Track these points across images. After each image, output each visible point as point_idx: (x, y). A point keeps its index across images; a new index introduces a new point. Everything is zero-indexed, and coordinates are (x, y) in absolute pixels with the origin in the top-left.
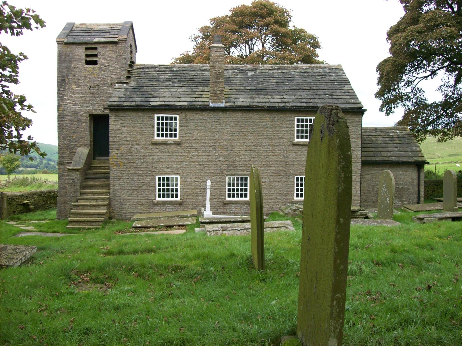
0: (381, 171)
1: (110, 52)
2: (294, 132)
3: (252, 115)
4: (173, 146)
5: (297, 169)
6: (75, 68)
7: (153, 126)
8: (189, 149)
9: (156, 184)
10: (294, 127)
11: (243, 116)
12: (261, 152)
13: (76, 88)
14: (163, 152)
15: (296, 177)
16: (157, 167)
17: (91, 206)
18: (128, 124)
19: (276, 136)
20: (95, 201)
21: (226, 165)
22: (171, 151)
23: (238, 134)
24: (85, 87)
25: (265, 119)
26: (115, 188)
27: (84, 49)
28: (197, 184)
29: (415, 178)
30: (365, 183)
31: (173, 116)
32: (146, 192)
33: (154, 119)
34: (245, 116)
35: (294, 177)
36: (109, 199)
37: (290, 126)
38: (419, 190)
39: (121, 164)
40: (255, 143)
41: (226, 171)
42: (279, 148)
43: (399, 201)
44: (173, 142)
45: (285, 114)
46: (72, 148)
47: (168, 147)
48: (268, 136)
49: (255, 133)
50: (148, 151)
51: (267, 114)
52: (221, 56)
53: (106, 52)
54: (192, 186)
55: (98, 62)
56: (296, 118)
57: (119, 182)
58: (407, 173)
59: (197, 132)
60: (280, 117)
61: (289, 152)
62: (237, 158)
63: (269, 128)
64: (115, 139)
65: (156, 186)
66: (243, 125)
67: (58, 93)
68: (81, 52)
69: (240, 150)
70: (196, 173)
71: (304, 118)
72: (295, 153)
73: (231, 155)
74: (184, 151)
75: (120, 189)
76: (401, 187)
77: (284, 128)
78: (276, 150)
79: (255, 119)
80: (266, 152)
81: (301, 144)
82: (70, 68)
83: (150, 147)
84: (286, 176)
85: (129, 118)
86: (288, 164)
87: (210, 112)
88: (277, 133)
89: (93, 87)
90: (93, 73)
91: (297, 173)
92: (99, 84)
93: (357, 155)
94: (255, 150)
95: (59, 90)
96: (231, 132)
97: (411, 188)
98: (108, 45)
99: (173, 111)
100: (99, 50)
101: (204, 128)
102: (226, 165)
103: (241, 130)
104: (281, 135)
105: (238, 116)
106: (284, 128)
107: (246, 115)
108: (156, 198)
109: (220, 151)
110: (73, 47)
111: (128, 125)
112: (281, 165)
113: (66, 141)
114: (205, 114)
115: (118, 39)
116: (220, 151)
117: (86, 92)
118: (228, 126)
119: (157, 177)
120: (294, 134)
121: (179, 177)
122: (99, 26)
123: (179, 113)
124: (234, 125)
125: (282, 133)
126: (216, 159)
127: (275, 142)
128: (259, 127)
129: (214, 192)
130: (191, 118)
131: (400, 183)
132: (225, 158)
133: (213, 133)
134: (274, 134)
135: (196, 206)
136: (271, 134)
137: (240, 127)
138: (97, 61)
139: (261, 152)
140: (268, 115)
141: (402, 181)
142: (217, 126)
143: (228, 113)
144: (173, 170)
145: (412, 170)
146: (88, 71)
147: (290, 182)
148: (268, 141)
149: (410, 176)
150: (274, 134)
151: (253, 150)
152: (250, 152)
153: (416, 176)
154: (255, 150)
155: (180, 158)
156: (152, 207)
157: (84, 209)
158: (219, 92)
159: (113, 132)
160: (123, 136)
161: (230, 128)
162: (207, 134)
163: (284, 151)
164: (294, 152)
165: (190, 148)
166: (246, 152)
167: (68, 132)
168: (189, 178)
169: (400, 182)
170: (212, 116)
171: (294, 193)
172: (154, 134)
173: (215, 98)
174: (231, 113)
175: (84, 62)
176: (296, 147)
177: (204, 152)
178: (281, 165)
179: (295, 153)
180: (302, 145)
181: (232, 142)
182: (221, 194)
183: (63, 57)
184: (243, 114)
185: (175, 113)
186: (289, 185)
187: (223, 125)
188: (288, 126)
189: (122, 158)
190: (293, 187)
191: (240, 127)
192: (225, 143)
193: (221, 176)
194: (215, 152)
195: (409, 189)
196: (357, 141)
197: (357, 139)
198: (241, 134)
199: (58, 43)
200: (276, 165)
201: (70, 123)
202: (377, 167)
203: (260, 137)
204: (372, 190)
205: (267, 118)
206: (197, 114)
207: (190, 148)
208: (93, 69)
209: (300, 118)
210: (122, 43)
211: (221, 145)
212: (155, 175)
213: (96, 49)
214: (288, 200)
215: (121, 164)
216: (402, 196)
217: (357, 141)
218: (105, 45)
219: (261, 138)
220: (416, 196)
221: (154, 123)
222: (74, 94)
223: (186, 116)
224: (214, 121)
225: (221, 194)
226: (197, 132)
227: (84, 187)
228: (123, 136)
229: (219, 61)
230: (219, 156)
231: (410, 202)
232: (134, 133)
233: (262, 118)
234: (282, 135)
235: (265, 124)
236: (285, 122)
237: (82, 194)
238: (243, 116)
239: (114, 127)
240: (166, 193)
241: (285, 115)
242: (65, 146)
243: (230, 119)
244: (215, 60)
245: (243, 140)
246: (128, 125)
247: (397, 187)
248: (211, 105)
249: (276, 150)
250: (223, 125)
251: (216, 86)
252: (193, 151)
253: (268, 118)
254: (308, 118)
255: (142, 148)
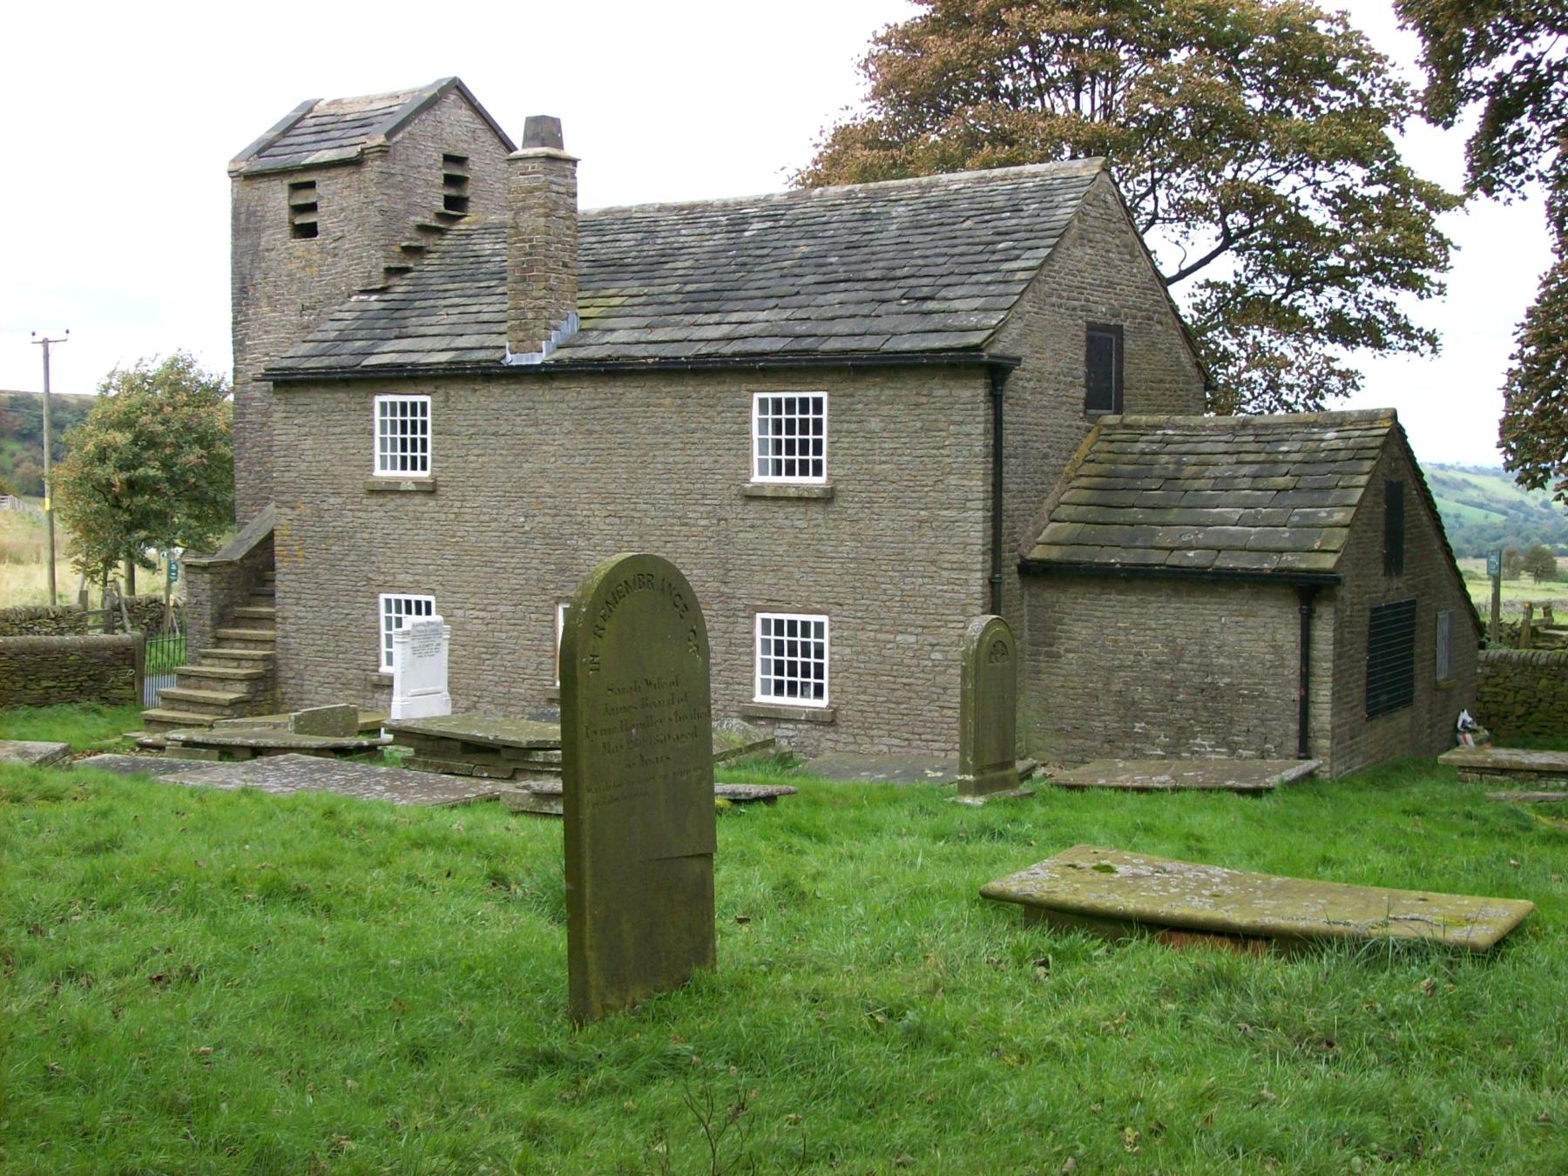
0: (1135, 610)
1: (346, 192)
2: (750, 449)
3: (621, 391)
4: (418, 500)
5: (759, 586)
6: (267, 250)
7: (372, 433)
8: (457, 510)
9: (378, 621)
10: (749, 432)
11: (597, 393)
12: (649, 521)
13: (272, 311)
14: (395, 518)
15: (759, 616)
16: (382, 565)
17: (214, 679)
18: (313, 427)
19: (693, 466)
20: (235, 664)
21: (553, 567)
22: (411, 515)
23: (582, 459)
24: (291, 307)
25: (660, 405)
26: (289, 627)
27: (286, 187)
28: (477, 626)
29: (1287, 646)
30: (1071, 655)
31: (811, 395)
32: (356, 645)
33: (371, 409)
34: (602, 396)
35: (752, 618)
36: (265, 659)
37: (735, 428)
38: (1305, 703)
39: (299, 553)
40: (632, 491)
41: (552, 586)
42: (702, 509)
43: (1218, 745)
44: (412, 487)
45: (719, 383)
46: (264, 498)
47: (404, 500)
48: (669, 467)
49: (630, 455)
50: (360, 514)
51: (665, 386)
52: (536, 189)
53: (334, 193)
54: (467, 633)
55: (319, 229)
56: (757, 396)
57: (296, 608)
58: (1250, 622)
59: (476, 452)
60: (703, 393)
61: (735, 526)
62: (582, 543)
63: (671, 436)
64: (286, 474)
65: (379, 627)
66: (598, 428)
67: (234, 330)
68: (278, 197)
69: (590, 513)
70: (476, 590)
71: (784, 395)
72: (752, 526)
73: (567, 530)
74: (443, 517)
75: (297, 630)
76: (1227, 680)
77: (719, 434)
78: (694, 515)
79: (632, 405)
80: (662, 522)
81: (768, 493)
82: (256, 253)
83: (365, 501)
84: (728, 613)
85: (315, 407)
86: (730, 566)
87: (508, 384)
88: (697, 452)
89: (308, 308)
90: (309, 264)
91: (759, 603)
92: (322, 298)
93: (969, 541)
94: (633, 513)
95: (236, 323)
96: (565, 453)
97: (1272, 691)
98: (339, 171)
99: (416, 385)
100: (319, 189)
101: (493, 440)
102: (553, 567)
103: (592, 446)
104: (708, 462)
105: (582, 395)
106: (719, 434)
107: (606, 390)
108: (379, 666)
109: (534, 516)
110: (263, 185)
111: (314, 430)
112: (710, 572)
113: (252, 477)
114: (496, 390)
115: (359, 148)
116: (534, 516)
117: (292, 324)
118: (557, 429)
119: (383, 597)
120: (748, 457)
121: (824, 619)
122: (371, 102)
123: (432, 389)
124: (572, 428)
125: (712, 452)
126: (526, 543)
127: (690, 486)
128: (643, 431)
129: (524, 658)
130: (460, 407)
131: (1222, 666)
132: (550, 541)
133: (517, 455)
134: (687, 459)
135: (475, 699)
136: (677, 459)
137: (590, 432)
138: (315, 224)
139: (649, 521)
140: (668, 389)
141: (1229, 657)
142: (526, 429)
143: (556, 384)
144: (417, 578)
145: (1274, 611)
146: (299, 258)
147: (738, 636)
148: (668, 482)
149: (1268, 637)
150: (687, 459)
151: (625, 513)
152: (617, 521)
153: (1292, 638)
154: (633, 513)
155: (433, 540)
156: (369, 695)
157: (200, 688)
158: (530, 315)
159: (282, 453)
160: (303, 466)
161: (562, 436)
162: (500, 458)
163: (719, 520)
164: (748, 523)
165: (459, 504)
166: (607, 521)
167: (257, 449)
168: (458, 605)
169: (1222, 660)
170: (514, 398)
171: (752, 679)
172: (372, 460)
173: (521, 335)
174: (563, 385)
175: (287, 229)
176: (754, 506)
177: (496, 520)
178: (710, 572)
179: (752, 526)
180: (775, 499)
181: (569, 487)
182: (541, 663)
183: (243, 217)
184: (595, 389)
185: (420, 388)
186: (736, 645)
187: (544, 428)
188: (728, 426)
189: (302, 533)
190: (748, 654)
191: (590, 432)
192: (548, 489)
193: (541, 604)
194: (522, 519)
195: (1262, 693)
196: (966, 482)
197: (967, 474)
198: (591, 458)
199: (235, 175)
200: (695, 572)
201: (259, 420)
202: (1120, 593)
203: (645, 467)
204: (1100, 685)
205: (665, 398)
206: (476, 390)
207: (459, 504)
208: (308, 250)
209: (769, 396)
210: (372, 160)
211: (537, 498)
212: (376, 590)
213: (311, 185)
214: (735, 703)
215: (299, 553)
216: (1231, 721)
217: (966, 482)
218: (332, 173)
219: (648, 471)
220: (1294, 727)
221: (373, 425)
222: (266, 332)
223: (447, 400)
224: (520, 415)
225: (541, 663)
226: (476, 452)
227: (221, 619)
228: (303, 466)
229: (531, 208)
230: (532, 535)
231: (1268, 751)
232: (329, 457)
233: (653, 401)
234: (711, 459)
235: (659, 420)
236: (719, 413)
237: (219, 641)
238: (597, 393)
239: (283, 438)
240: (786, 678)
241: (719, 388)
242: (250, 492)
243: (561, 405)
244: (520, 204)
245: (598, 480)
246: (314, 430)
247: (1209, 680)
248: (512, 359)
249: (694, 515)
250: (544, 428)
251: (524, 293)
252: (467, 517)
253: (668, 401)
254: (797, 395)
255: (344, 503)
